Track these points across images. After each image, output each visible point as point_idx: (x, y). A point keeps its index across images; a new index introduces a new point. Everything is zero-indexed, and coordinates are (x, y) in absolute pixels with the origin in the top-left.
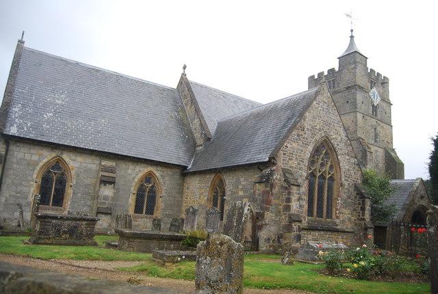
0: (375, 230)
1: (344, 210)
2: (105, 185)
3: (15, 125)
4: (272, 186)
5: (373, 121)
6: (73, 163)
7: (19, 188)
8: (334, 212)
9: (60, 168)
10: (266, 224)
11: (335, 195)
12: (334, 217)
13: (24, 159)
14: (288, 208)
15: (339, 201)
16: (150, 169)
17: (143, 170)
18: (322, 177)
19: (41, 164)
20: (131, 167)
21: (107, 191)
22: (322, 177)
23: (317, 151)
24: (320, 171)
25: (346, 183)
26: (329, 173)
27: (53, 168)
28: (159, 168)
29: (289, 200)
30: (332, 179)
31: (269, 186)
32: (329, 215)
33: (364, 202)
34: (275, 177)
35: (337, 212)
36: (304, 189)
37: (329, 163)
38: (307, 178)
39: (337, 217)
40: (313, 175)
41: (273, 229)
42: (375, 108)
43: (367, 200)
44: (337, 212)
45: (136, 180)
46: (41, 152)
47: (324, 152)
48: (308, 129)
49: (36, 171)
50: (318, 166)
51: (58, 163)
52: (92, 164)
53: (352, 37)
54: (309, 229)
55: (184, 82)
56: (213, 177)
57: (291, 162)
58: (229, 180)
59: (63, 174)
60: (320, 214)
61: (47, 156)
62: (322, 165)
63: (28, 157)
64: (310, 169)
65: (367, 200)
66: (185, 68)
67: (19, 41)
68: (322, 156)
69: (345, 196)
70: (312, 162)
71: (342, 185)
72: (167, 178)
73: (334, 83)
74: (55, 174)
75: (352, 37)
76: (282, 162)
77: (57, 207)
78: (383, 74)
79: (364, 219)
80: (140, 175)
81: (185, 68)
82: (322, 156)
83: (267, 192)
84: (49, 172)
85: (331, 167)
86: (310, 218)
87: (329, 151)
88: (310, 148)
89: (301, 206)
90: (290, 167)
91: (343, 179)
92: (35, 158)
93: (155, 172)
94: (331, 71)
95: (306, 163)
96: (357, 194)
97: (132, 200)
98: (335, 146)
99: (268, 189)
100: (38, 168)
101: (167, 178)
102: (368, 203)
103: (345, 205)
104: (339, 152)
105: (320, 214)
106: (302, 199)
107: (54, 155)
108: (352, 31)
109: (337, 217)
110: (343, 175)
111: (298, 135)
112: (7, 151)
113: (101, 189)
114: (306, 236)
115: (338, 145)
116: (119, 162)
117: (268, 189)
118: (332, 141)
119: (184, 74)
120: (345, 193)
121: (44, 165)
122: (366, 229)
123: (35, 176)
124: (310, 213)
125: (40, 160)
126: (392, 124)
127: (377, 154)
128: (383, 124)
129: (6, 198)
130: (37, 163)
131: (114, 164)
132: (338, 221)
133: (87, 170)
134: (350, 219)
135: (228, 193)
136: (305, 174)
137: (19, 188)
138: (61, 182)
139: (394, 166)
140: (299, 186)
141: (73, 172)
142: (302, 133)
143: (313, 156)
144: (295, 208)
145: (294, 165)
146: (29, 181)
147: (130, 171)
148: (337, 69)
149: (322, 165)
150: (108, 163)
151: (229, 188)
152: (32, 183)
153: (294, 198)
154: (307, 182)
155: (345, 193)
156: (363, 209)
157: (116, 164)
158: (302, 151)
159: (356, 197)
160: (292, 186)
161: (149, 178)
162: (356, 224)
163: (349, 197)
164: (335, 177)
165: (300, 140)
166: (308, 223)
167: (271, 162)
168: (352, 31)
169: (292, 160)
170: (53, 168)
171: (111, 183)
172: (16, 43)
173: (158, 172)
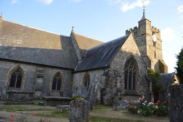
0: (154, 95)
1: (140, 87)
2: (39, 78)
4: (109, 77)
5: (154, 48)
8: (136, 88)
10: (107, 93)
11: (136, 80)
12: (136, 89)
14: (116, 86)
15: (138, 83)
17: (56, 71)
18: (131, 72)
19: (11, 70)
20: (50, 70)
21: (40, 81)
22: (131, 72)
23: (128, 61)
24: (129, 70)
25: (141, 75)
26: (133, 71)
27: (16, 71)
28: (63, 70)
29: (116, 83)
30: (135, 73)
32: (134, 89)
33: (149, 83)
35: (138, 87)
36: (123, 77)
37: (134, 67)
38: (124, 73)
39: (138, 90)
40: (126, 72)
41: (109, 95)
42: (154, 43)
43: (150, 82)
44: (138, 87)
45: (52, 76)
46: (11, 64)
47: (131, 62)
49: (8, 73)
50: (129, 68)
51: (18, 69)
52: (33, 69)
53: (144, 13)
54: (126, 95)
55: (72, 34)
58: (91, 74)
59: (21, 74)
60: (130, 88)
62: (131, 67)
63: (5, 67)
64: (125, 69)
65: (150, 82)
68: (130, 64)
69: (141, 80)
70: (126, 66)
71: (139, 76)
73: (137, 33)
74: (17, 74)
75: (144, 13)
78: (158, 28)
79: (149, 90)
80: (54, 73)
81: (73, 28)
82: (130, 64)
83: (107, 79)
84: (15, 73)
85: (134, 68)
86: (126, 90)
87: (133, 62)
88: (125, 60)
89: (121, 85)
90: (117, 69)
91: (140, 73)
92: (8, 67)
93: (61, 72)
94: (135, 28)
95: (123, 66)
96: (146, 80)
97: (51, 84)
98: (136, 59)
99: (107, 78)
100: (9, 71)
101: (66, 75)
102: (151, 83)
103: (141, 84)
104: (138, 62)
105: (130, 88)
107: (16, 66)
108: (144, 10)
109: (138, 90)
110: (140, 72)
111: (120, 55)
114: (124, 98)
115: (137, 59)
117: (107, 78)
118: (135, 57)
120: (141, 79)
122: (150, 95)
123: (8, 75)
124: (126, 88)
125: (10, 68)
126: (162, 50)
127: (154, 62)
128: (158, 50)
130: (9, 70)
131: (43, 69)
132: (138, 91)
134: (143, 91)
135: (91, 80)
136: (123, 71)
139: (161, 66)
140: (120, 76)
141: (25, 73)
142: (121, 54)
143: (126, 64)
144: (119, 86)
145: (118, 68)
146: (5, 77)
147: (50, 72)
148: (138, 27)
149: (131, 67)
150: (40, 69)
151: (91, 78)
152: (6, 78)
153: (118, 82)
154: (124, 75)
155: (141, 79)
156: (149, 86)
158: (121, 62)
159: (145, 81)
161: (58, 74)
162: (146, 93)
163: (142, 81)
164: (136, 72)
166: (125, 92)
167: (108, 67)
168: (144, 10)
169: (117, 65)
171: (41, 77)
173: (62, 72)
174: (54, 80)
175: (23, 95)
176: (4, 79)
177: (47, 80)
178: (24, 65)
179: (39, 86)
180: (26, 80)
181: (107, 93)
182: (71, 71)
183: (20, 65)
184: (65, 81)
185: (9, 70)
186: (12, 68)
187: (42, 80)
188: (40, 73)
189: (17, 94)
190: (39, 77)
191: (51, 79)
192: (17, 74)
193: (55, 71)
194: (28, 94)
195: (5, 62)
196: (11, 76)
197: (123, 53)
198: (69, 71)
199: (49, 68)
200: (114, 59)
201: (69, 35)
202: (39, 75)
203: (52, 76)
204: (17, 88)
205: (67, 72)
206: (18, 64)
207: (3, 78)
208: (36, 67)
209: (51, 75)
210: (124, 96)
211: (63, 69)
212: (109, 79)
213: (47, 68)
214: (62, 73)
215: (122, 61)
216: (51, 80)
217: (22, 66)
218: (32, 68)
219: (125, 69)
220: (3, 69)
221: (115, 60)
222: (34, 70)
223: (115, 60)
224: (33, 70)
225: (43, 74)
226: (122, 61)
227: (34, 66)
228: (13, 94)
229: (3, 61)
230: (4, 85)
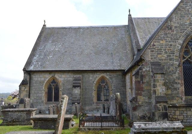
2: (75, 88)
3: (33, 65)
4: (142, 77)
6: (60, 78)
7: (38, 95)
9: (55, 83)
10: (140, 106)
13: (38, 81)
14: (155, 92)
16: (102, 75)
17: (99, 76)
19: (46, 82)
20: (91, 76)
21: (77, 91)
27: (52, 83)
28: (108, 74)
29: (155, 86)
31: (139, 77)
34: (144, 70)
38: (179, 66)
41: (147, 108)
45: (95, 82)
46: (45, 76)
48: (176, 27)
49: (44, 86)
51: (54, 80)
52: (70, 77)
56: (130, 74)
57: (159, 56)
59: (57, 85)
61: (48, 77)
63: (39, 79)
64: (184, 58)
66: (129, 11)
67: (129, 15)
72: (114, 79)
74: (53, 85)
76: (150, 57)
77: (56, 102)
80: (97, 79)
81: (129, 11)
83: (139, 82)
84: (51, 85)
90: (160, 60)
92: (43, 79)
93: (106, 76)
97: (94, 94)
99: (139, 79)
100: (45, 84)
101: (114, 79)
106: (176, 83)
107: (51, 76)
111: (166, 34)
112: (30, 79)
113: (74, 90)
114: (185, 112)
116: (84, 74)
119: (130, 15)
121: (47, 82)
123: (44, 88)
125: (45, 80)
129: (33, 100)
130: (44, 82)
131: (81, 76)
133: (68, 81)
136: (177, 63)
137: (38, 95)
138: (57, 89)
141: (61, 84)
142: (168, 31)
144: (160, 91)
145: (163, 58)
146: (41, 91)
147: (91, 78)
150: (77, 76)
152: (43, 91)
157: (83, 76)
158: (171, 45)
160: (155, 75)
161: (103, 80)
165: (168, 37)
169: (161, 54)
170: (52, 83)
171: (78, 86)
172: (42, 26)
173: (107, 76)
174: (98, 88)
175: (19, 114)
176: (40, 93)
177: (89, 89)
178: (59, 74)
179: (76, 98)
180: (63, 92)
181: (140, 106)
182: (121, 73)
183: (55, 75)
184: (114, 87)
185: (44, 82)
186: (47, 80)
187: (79, 90)
188: (77, 82)
189: (12, 113)
190: (75, 87)
191: (94, 88)
192: (53, 85)
193: (97, 76)
194: (25, 113)
195: (38, 74)
196: (48, 88)
197: (173, 28)
198: (118, 73)
199: (89, 74)
200: (152, 44)
201: (126, 23)
202: (75, 85)
203: (95, 82)
204: (55, 102)
205: (115, 75)
206: (52, 74)
207: (39, 92)
208: (72, 74)
209: (93, 82)
210: (184, 109)
211: (108, 72)
212: (142, 80)
213: (86, 74)
214: (108, 77)
215: (172, 43)
216: (94, 88)
217: (57, 76)
218: (68, 76)
219: (184, 58)
220: (38, 82)
221: (154, 45)
222: (71, 79)
223: (155, 45)
224: (70, 78)
225: (80, 82)
226: (172, 43)
227: (70, 74)
228: (7, 113)
229: (37, 73)
230: (41, 99)
